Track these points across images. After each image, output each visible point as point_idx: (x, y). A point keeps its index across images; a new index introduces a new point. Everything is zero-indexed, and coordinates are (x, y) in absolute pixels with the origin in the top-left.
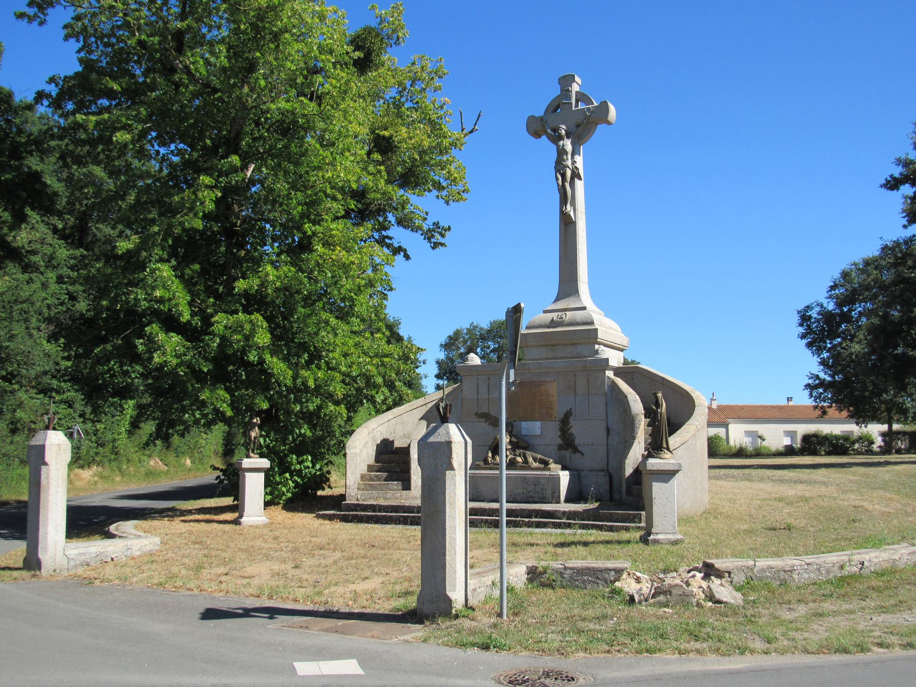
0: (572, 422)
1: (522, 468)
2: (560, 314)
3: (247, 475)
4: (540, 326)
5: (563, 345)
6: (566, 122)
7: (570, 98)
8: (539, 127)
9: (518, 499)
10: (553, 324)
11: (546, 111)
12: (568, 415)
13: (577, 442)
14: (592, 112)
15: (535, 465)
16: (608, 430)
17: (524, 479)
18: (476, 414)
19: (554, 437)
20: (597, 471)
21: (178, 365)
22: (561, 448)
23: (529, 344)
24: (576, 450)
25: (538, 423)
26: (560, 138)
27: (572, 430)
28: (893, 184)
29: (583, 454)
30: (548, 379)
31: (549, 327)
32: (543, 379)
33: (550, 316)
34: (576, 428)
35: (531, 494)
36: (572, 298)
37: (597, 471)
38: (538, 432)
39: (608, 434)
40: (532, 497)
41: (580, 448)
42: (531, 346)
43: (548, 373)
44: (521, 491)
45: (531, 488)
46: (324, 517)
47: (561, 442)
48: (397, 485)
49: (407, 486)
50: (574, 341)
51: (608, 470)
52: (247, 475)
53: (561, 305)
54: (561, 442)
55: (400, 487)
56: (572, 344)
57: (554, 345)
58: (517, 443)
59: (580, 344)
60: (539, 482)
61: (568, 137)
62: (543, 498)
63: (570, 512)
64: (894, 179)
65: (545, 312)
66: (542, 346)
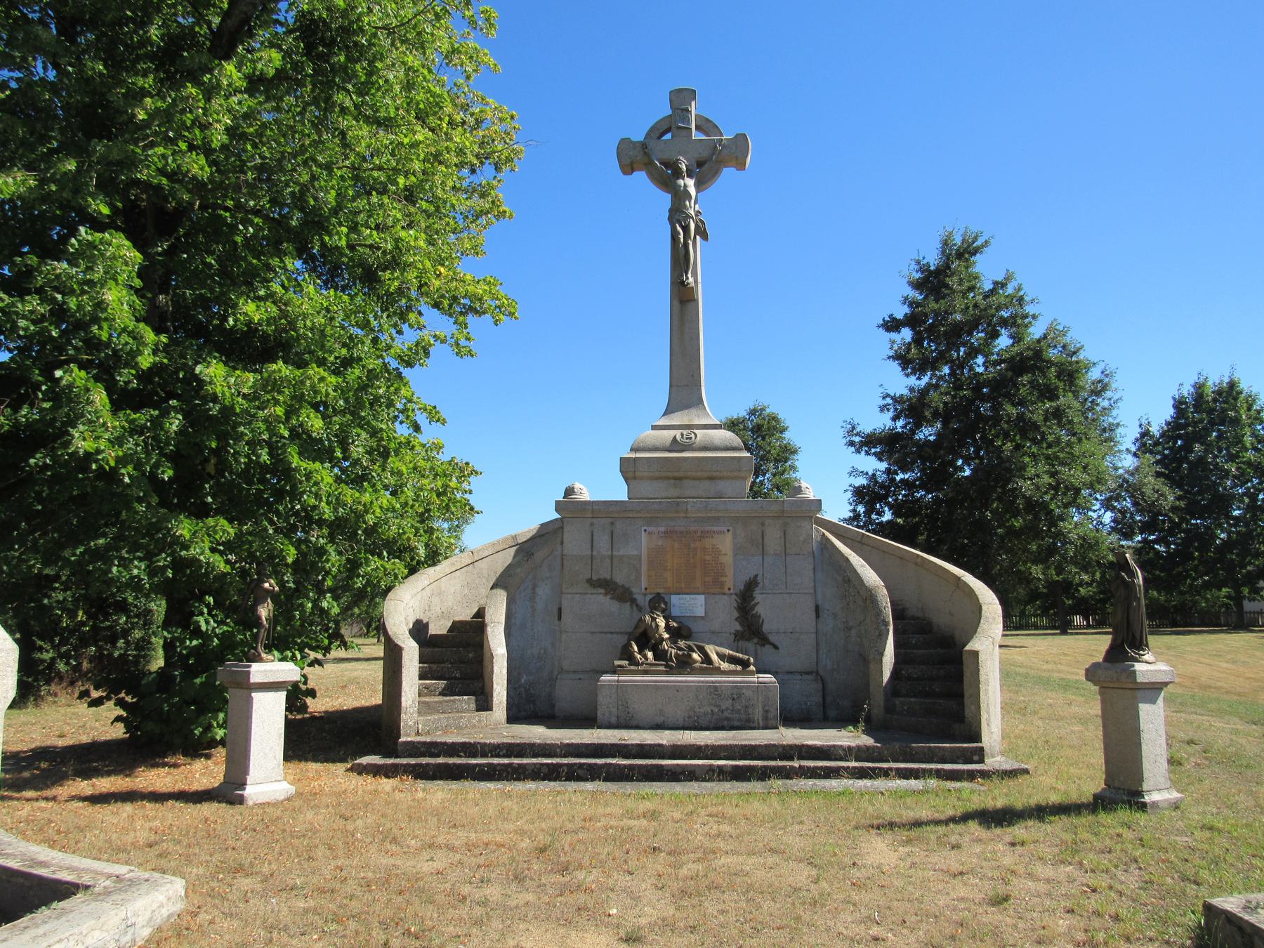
0: (758, 596)
1: (702, 671)
2: (685, 432)
3: (256, 696)
4: (655, 449)
5: (695, 479)
6: (677, 156)
7: (689, 122)
8: (635, 157)
9: (703, 723)
10: (675, 445)
11: (648, 135)
12: (751, 585)
13: (765, 628)
14: (724, 147)
15: (725, 666)
16: (817, 608)
17: (714, 689)
18: (590, 582)
19: (726, 616)
20: (801, 673)
21: (121, 461)
22: (738, 636)
23: (638, 474)
24: (764, 640)
25: (701, 599)
26: (678, 174)
27: (759, 610)
28: (892, 325)
29: (776, 647)
30: (716, 529)
31: (670, 451)
32: (708, 528)
33: (668, 435)
34: (764, 606)
35: (726, 714)
36: (694, 411)
37: (801, 673)
38: (700, 611)
39: (818, 616)
40: (728, 719)
41: (772, 638)
42: (642, 478)
43: (719, 518)
44: (708, 709)
45: (727, 704)
46: (361, 770)
47: (739, 628)
48: (467, 702)
49: (485, 704)
50: (715, 474)
51: (817, 673)
52: (256, 696)
53: (676, 419)
54: (739, 628)
55: (473, 706)
56: (711, 478)
57: (680, 479)
58: (679, 629)
59: (721, 478)
60: (740, 696)
61: (689, 176)
62: (748, 720)
63: (859, 747)
64: (893, 319)
65: (654, 428)
66: (668, 478)
